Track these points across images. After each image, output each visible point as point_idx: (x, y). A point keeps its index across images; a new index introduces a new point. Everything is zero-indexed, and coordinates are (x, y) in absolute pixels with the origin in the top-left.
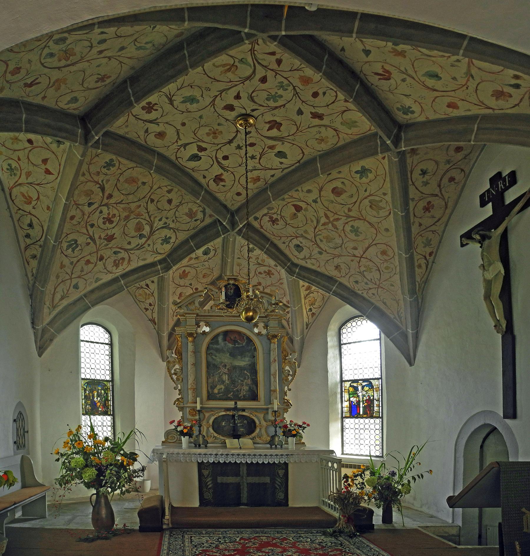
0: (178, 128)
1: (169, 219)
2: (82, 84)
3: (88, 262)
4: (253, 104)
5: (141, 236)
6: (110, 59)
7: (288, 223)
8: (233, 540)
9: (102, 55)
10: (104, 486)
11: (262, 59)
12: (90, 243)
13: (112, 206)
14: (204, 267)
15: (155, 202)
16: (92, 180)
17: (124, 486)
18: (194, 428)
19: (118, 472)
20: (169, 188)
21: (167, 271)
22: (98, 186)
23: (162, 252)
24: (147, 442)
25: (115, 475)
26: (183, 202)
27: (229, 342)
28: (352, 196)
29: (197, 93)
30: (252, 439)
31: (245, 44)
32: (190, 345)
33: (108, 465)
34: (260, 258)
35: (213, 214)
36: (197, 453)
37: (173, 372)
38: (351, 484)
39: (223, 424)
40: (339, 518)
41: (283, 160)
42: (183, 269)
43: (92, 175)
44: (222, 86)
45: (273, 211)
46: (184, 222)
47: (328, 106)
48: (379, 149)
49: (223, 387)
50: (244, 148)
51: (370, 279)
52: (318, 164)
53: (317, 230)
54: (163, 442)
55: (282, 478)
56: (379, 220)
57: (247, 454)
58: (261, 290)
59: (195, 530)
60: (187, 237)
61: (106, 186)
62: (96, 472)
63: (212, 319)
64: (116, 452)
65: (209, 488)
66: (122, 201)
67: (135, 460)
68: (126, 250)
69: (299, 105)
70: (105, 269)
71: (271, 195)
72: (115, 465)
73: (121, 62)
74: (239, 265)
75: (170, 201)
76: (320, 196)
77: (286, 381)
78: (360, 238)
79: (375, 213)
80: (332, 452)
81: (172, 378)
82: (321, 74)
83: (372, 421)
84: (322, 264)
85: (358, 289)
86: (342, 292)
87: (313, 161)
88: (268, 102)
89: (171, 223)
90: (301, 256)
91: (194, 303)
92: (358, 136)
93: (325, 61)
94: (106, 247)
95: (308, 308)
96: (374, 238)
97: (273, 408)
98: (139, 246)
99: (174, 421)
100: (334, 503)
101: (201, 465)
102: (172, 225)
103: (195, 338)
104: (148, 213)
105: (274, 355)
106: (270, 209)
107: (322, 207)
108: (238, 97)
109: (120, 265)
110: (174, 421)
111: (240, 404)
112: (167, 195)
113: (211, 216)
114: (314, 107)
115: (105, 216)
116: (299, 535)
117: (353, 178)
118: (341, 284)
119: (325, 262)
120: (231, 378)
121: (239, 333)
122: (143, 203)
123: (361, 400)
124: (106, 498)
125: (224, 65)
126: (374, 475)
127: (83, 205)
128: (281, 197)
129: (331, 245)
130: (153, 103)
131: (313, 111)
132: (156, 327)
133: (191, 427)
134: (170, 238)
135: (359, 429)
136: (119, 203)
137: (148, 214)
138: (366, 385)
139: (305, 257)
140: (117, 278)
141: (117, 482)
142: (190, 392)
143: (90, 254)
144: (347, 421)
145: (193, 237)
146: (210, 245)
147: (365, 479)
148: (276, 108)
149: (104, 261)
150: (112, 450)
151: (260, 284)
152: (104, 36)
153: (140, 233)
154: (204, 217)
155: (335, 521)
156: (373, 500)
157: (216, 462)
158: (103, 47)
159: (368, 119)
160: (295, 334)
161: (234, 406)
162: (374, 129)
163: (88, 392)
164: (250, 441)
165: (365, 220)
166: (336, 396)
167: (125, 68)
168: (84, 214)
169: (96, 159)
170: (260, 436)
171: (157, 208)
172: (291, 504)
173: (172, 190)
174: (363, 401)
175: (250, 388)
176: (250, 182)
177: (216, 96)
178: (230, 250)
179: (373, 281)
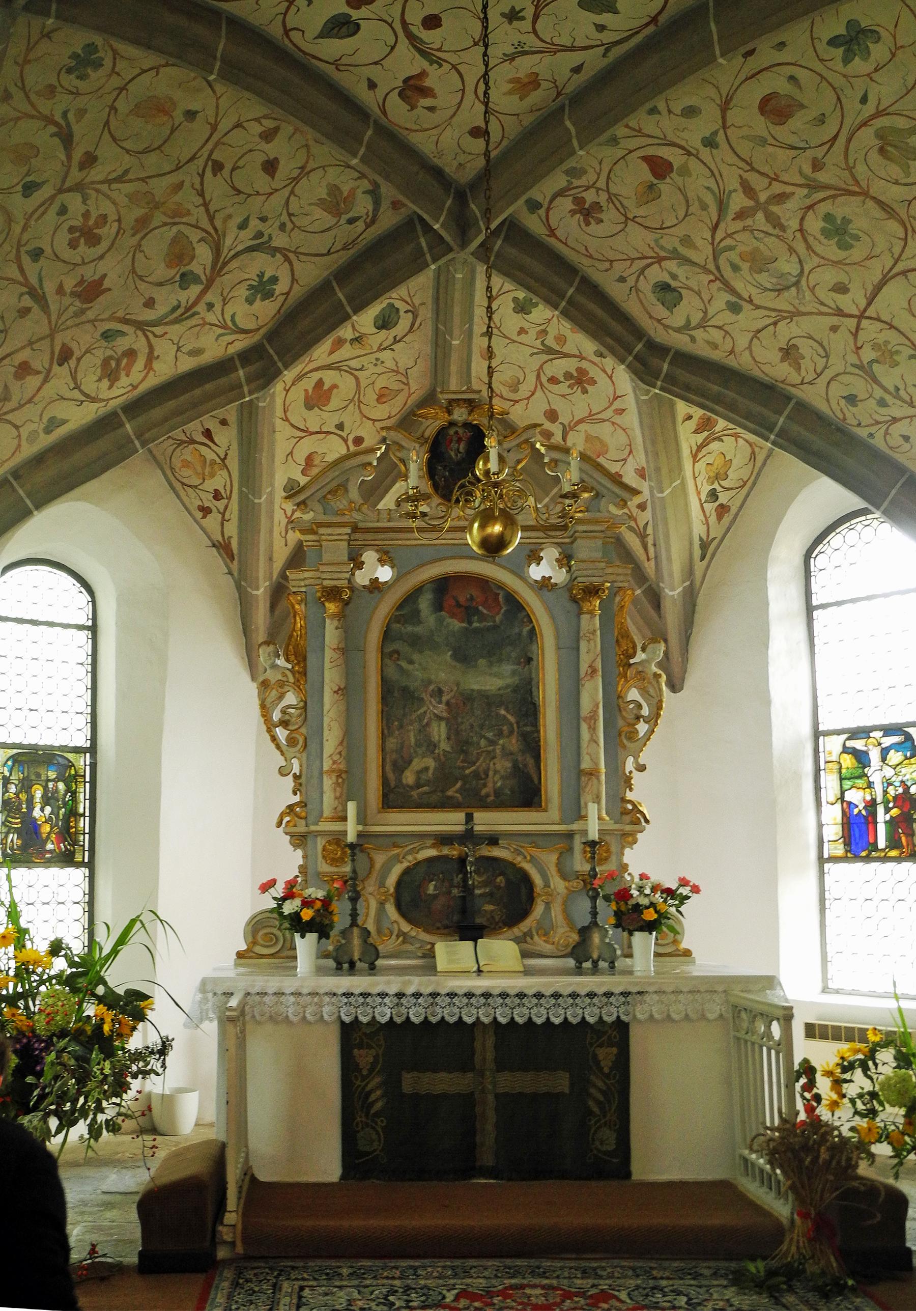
1: (270, 222)
3: (24, 369)
5: (186, 280)
7: (630, 216)
8: (434, 1297)
10: (35, 1108)
13: (97, 191)
14: (380, 369)
15: (226, 172)
18: (336, 906)
20: (269, 124)
22: (52, 129)
26: (311, 165)
27: (453, 615)
28: (821, 120)
30: (517, 940)
32: (330, 626)
33: (54, 1035)
34: (553, 331)
35: (401, 198)
36: (340, 991)
37: (276, 716)
39: (431, 889)
40: (792, 1221)
41: (606, 18)
43: (33, 96)
45: (583, 181)
46: (316, 227)
49: (431, 763)
51: (892, 389)
53: (720, 234)
55: (607, 1076)
59: (319, 1262)
60: (326, 273)
61: (75, 128)
63: (401, 540)
65: (377, 1114)
66: (126, 172)
67: (140, 1016)
68: (140, 326)
70: (77, 387)
75: (270, 167)
76: (724, 127)
78: (857, 253)
79: (895, 171)
81: (274, 739)
84: (742, 341)
85: (862, 419)
86: (805, 434)
89: (275, 232)
94: (77, 321)
95: (706, 489)
96: (897, 250)
97: (585, 832)
100: (770, 1162)
102: (280, 240)
103: (347, 603)
104: (206, 205)
105: (590, 652)
106: (574, 173)
107: (733, 159)
109: (123, 373)
110: (272, 883)
112: (264, 146)
116: (652, 1283)
117: (822, 60)
120: (457, 732)
122: (189, 176)
123: (879, 800)
129: (764, 279)
132: (235, 566)
133: (326, 902)
134: (274, 280)
137: (207, 211)
138: (897, 747)
139: (688, 321)
140: (114, 414)
143: (31, 343)
145: (343, 274)
146: (398, 296)
149: (73, 362)
150: (69, 981)
151: (552, 415)
153: (183, 270)
154: (376, 209)
155: (777, 1232)
157: (398, 1020)
161: (461, 828)
163: (13, 789)
165: (865, 194)
169: (44, 47)
170: (545, 930)
171: (234, 188)
173: (276, 130)
174: (886, 802)
175: (515, 766)
178: (457, 310)
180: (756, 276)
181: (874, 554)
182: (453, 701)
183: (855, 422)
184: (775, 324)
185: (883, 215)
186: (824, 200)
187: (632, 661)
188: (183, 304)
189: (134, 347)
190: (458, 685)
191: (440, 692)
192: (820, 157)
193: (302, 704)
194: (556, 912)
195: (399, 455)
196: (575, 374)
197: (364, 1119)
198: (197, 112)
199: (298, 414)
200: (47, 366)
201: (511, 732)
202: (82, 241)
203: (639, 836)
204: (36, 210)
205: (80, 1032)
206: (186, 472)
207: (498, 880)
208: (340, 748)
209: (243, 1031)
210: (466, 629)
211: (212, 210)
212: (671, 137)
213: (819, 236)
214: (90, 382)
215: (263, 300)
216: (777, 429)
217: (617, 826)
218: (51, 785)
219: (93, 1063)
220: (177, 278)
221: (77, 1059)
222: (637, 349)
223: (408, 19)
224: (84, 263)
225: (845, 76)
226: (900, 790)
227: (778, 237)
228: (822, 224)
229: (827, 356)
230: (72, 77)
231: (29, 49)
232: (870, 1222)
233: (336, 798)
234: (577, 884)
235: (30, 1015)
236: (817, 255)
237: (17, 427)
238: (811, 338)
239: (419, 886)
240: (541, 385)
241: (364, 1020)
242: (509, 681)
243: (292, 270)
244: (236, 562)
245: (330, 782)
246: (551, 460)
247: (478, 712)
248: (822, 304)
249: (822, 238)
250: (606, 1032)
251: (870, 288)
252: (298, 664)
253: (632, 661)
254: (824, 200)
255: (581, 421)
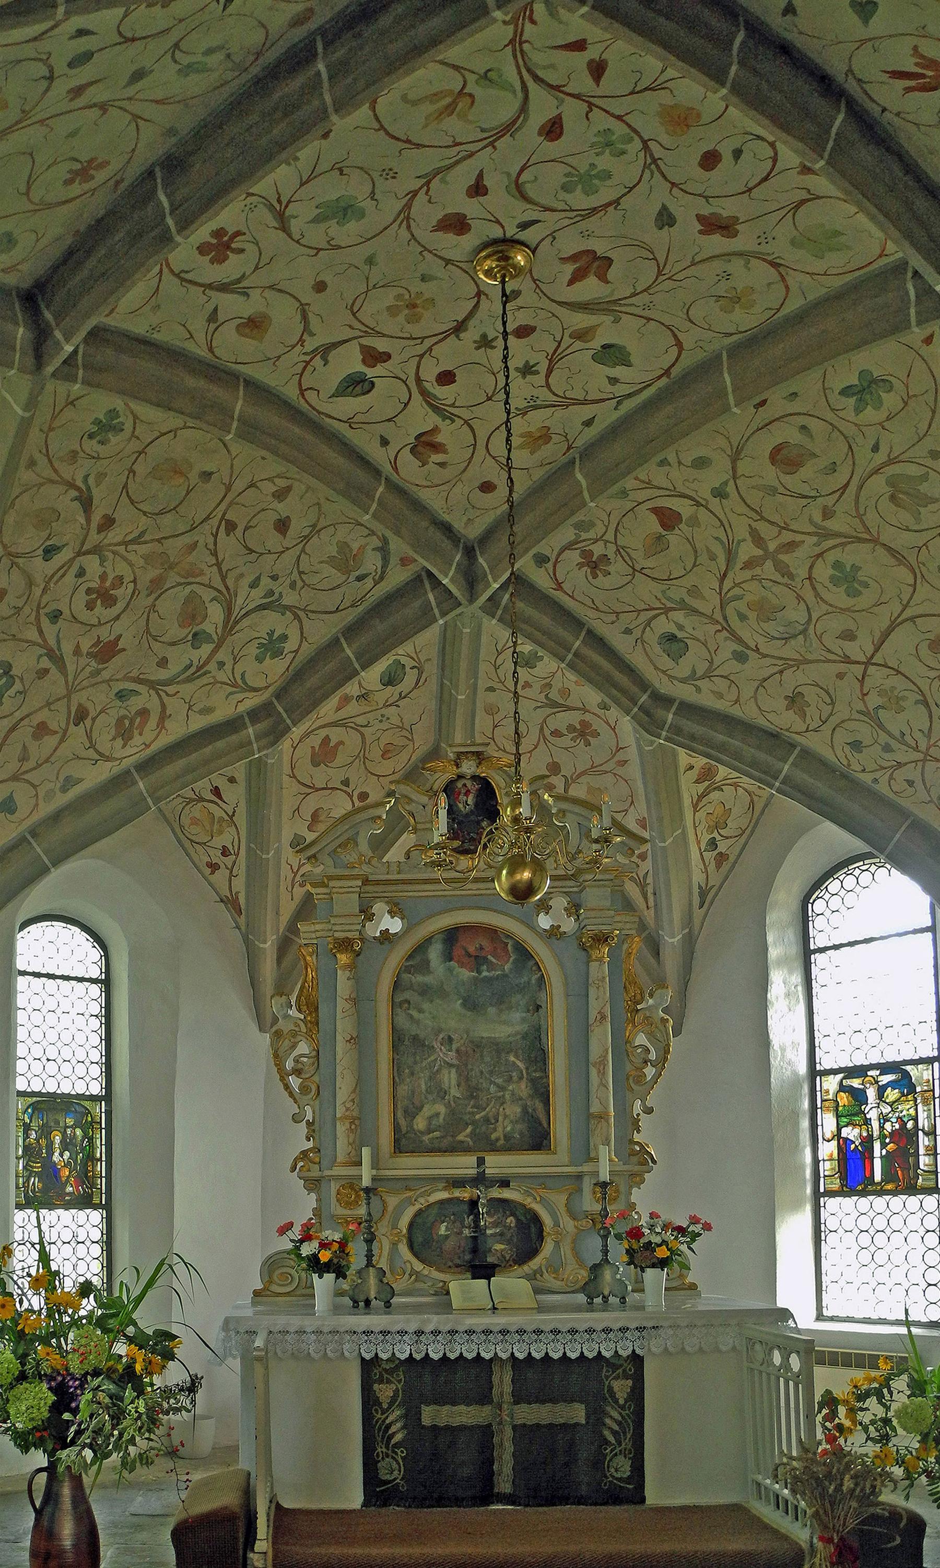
0: (303, 301)
1: (280, 580)
2: (27, 194)
3: (42, 730)
4: (521, 205)
5: (197, 639)
6: (105, 111)
7: (638, 567)
9: (81, 101)
10: (73, 1443)
11: (544, 68)
12: (46, 671)
13: (114, 553)
14: (385, 725)
16: (54, 477)
17: (132, 1441)
18: (351, 1247)
19: (116, 1398)
20: (282, 483)
21: (273, 744)
22: (74, 493)
23: (259, 683)
24: (207, 1304)
25: (108, 1408)
27: (462, 965)
28: (833, 468)
29: (355, 188)
31: (495, 20)
33: (87, 1373)
34: (557, 684)
35: (411, 553)
36: (361, 1330)
37: (289, 1065)
38: (847, 1423)
39: (442, 1230)
41: (618, 371)
42: (323, 733)
44: (429, 160)
45: (591, 534)
46: (325, 585)
47: (750, 190)
48: (913, 311)
49: (441, 1109)
50: (500, 343)
51: (897, 734)
52: (726, 375)
53: (727, 584)
54: (256, 1293)
55: (622, 1407)
56: (920, 539)
57: (513, 1329)
58: (560, 789)
60: (334, 630)
61: (95, 492)
62: (52, 1398)
63: (412, 892)
64: (111, 1331)
65: (397, 1445)
67: (169, 1356)
68: (153, 685)
69: (661, 195)
70: (92, 746)
71: (584, 483)
72: (110, 1373)
73: (136, 117)
74: (491, 710)
75: (282, 526)
76: (735, 478)
77: (638, 1082)
78: (864, 601)
79: (905, 517)
80: (786, 1314)
81: (287, 1087)
82: (724, 91)
83: (913, 1202)
84: (747, 691)
87: (708, 367)
88: (567, 197)
89: (286, 591)
90: (683, 669)
91: (356, 844)
92: (848, 278)
93: (735, 51)
94: (93, 681)
95: (705, 838)
96: (905, 598)
97: (596, 1174)
98: (193, 669)
99: (291, 1224)
100: (794, 1492)
101: (369, 1366)
102: (290, 599)
104: (218, 565)
106: (581, 526)
108: (478, 189)
109: (136, 732)
110: (290, 1226)
111: (496, 1164)
112: (276, 505)
113: (405, 561)
114: (706, 198)
115: (94, 585)
117: (832, 410)
118: (806, 754)
119: (756, 684)
120: (467, 1079)
121: (492, 932)
122: (203, 536)
124: (77, 1482)
125: (435, 97)
126: (923, 1393)
127: (29, 555)
128: (616, 488)
129: (773, 628)
130: (231, 230)
131: (706, 211)
132: (242, 920)
133: (343, 1244)
134: (284, 638)
135: (872, 1231)
136: (135, 541)
137: (220, 570)
139: (694, 672)
140: (128, 772)
141: (113, 1428)
142: (341, 1129)
143: (48, 704)
144: (831, 1204)
145: (351, 631)
146: (402, 653)
147: (894, 1406)
148: (594, 211)
149: (88, 722)
150: (101, 1323)
151: (555, 768)
152: (84, 44)
154: (385, 566)
156: (923, 1478)
157: (418, 1357)
158: (85, 74)
159: (872, 218)
160: (666, 926)
161: (473, 1172)
162: (897, 250)
163: (33, 1135)
164: (525, 1285)
165: (875, 541)
166: (796, 1124)
167: (149, 132)
168: (30, 583)
169: (69, 413)
170: (555, 1267)
172: (652, 1496)
173: (288, 489)
174: (882, 1137)
176: (521, 447)
177: (415, 193)
178: (464, 665)
179: (908, 738)
180: (762, 624)
181: (876, 900)
182: (463, 1048)
183: (860, 768)
184: (781, 672)
185: (893, 561)
186: (834, 547)
187: (639, 1007)
188: (195, 663)
189: (148, 706)
190: (467, 1033)
191: (450, 1040)
192: (830, 504)
193: (314, 1053)
194: (566, 1250)
195: (407, 808)
196: (578, 727)
197: (384, 1450)
198: (211, 474)
199: (305, 770)
200: (63, 726)
201: (521, 1078)
202: (99, 602)
203: (646, 1176)
204: (55, 573)
205: (111, 1370)
206: (194, 829)
207: (508, 1221)
208: (353, 1096)
209: (267, 1368)
210: (475, 978)
211: (224, 570)
212: (681, 489)
213: (828, 584)
214: (104, 740)
215: (272, 658)
216: (781, 777)
217: (626, 1167)
218: (69, 1131)
219: (127, 1401)
220: (190, 637)
221: (111, 1398)
222: (642, 700)
223: (423, 376)
224: (100, 624)
225: (856, 425)
226: (897, 1126)
227: (787, 585)
228: (831, 572)
229: (833, 703)
230: (94, 441)
231: (54, 417)
232: (889, 1545)
233: (350, 1144)
234: (586, 1223)
235: (63, 1354)
236: (826, 603)
237: (34, 786)
238: (818, 685)
239: (431, 1228)
240: (544, 738)
241: (384, 1356)
242: (518, 1028)
243: (301, 628)
244: (243, 917)
245: (344, 1129)
246: (559, 811)
247: (487, 1059)
248: (829, 651)
249: (830, 586)
250: (621, 1366)
251: (877, 635)
252: (310, 1013)
253: (639, 1007)
254: (834, 547)
255: (583, 773)
